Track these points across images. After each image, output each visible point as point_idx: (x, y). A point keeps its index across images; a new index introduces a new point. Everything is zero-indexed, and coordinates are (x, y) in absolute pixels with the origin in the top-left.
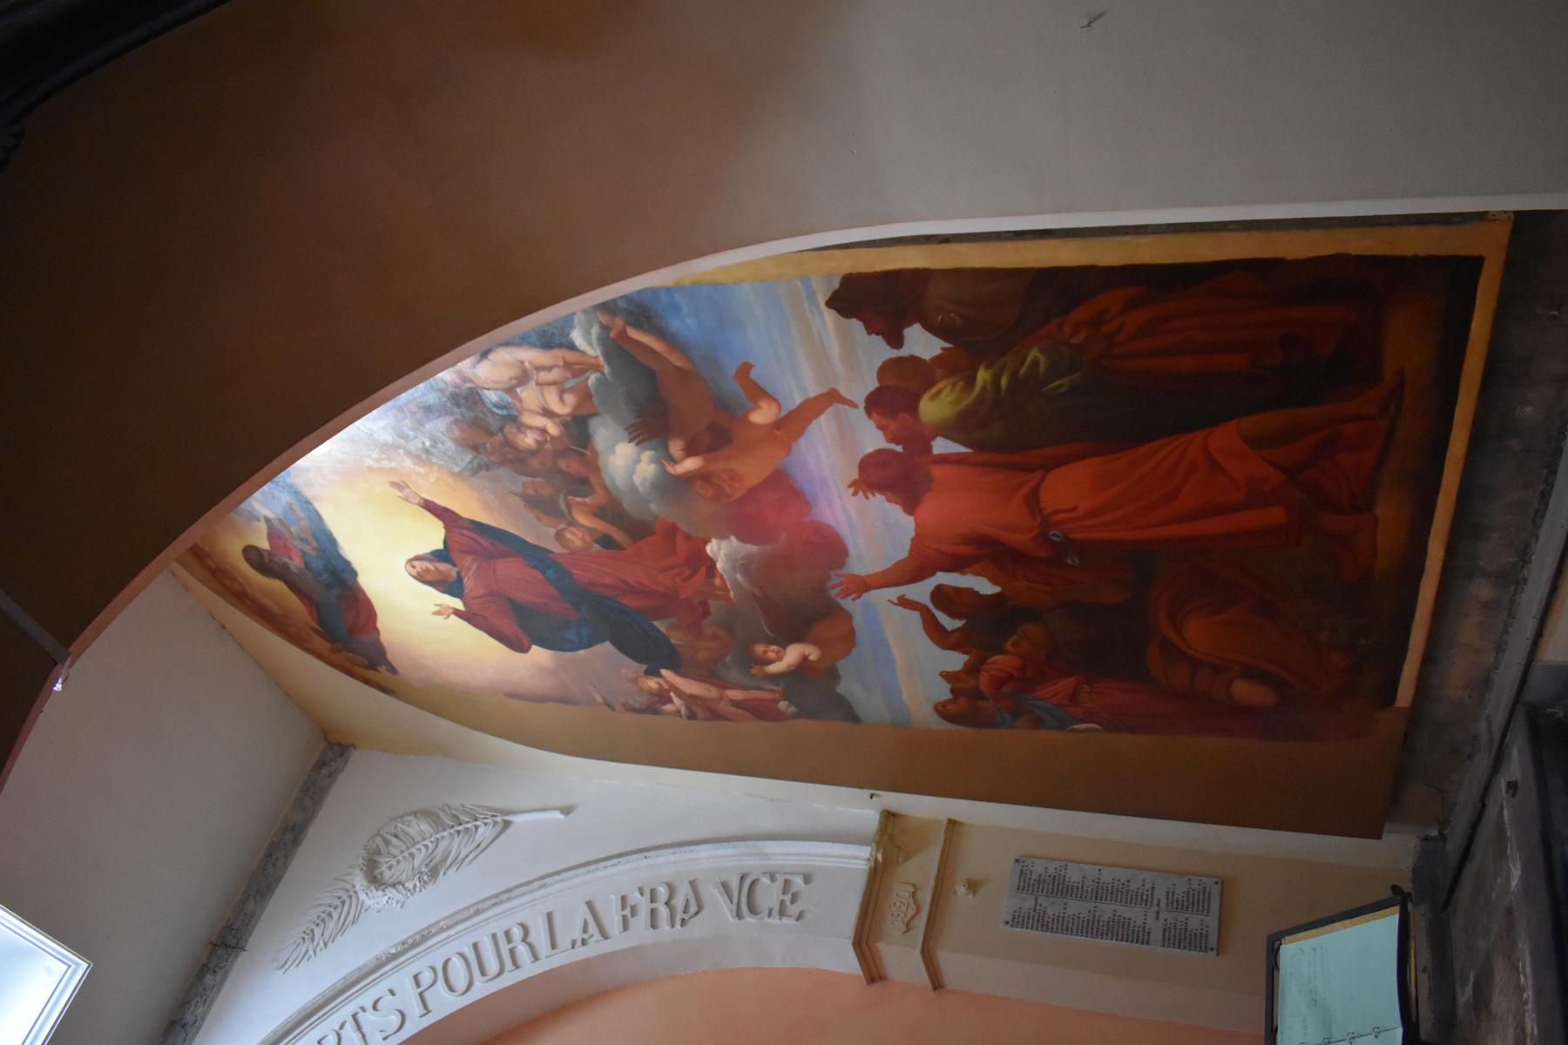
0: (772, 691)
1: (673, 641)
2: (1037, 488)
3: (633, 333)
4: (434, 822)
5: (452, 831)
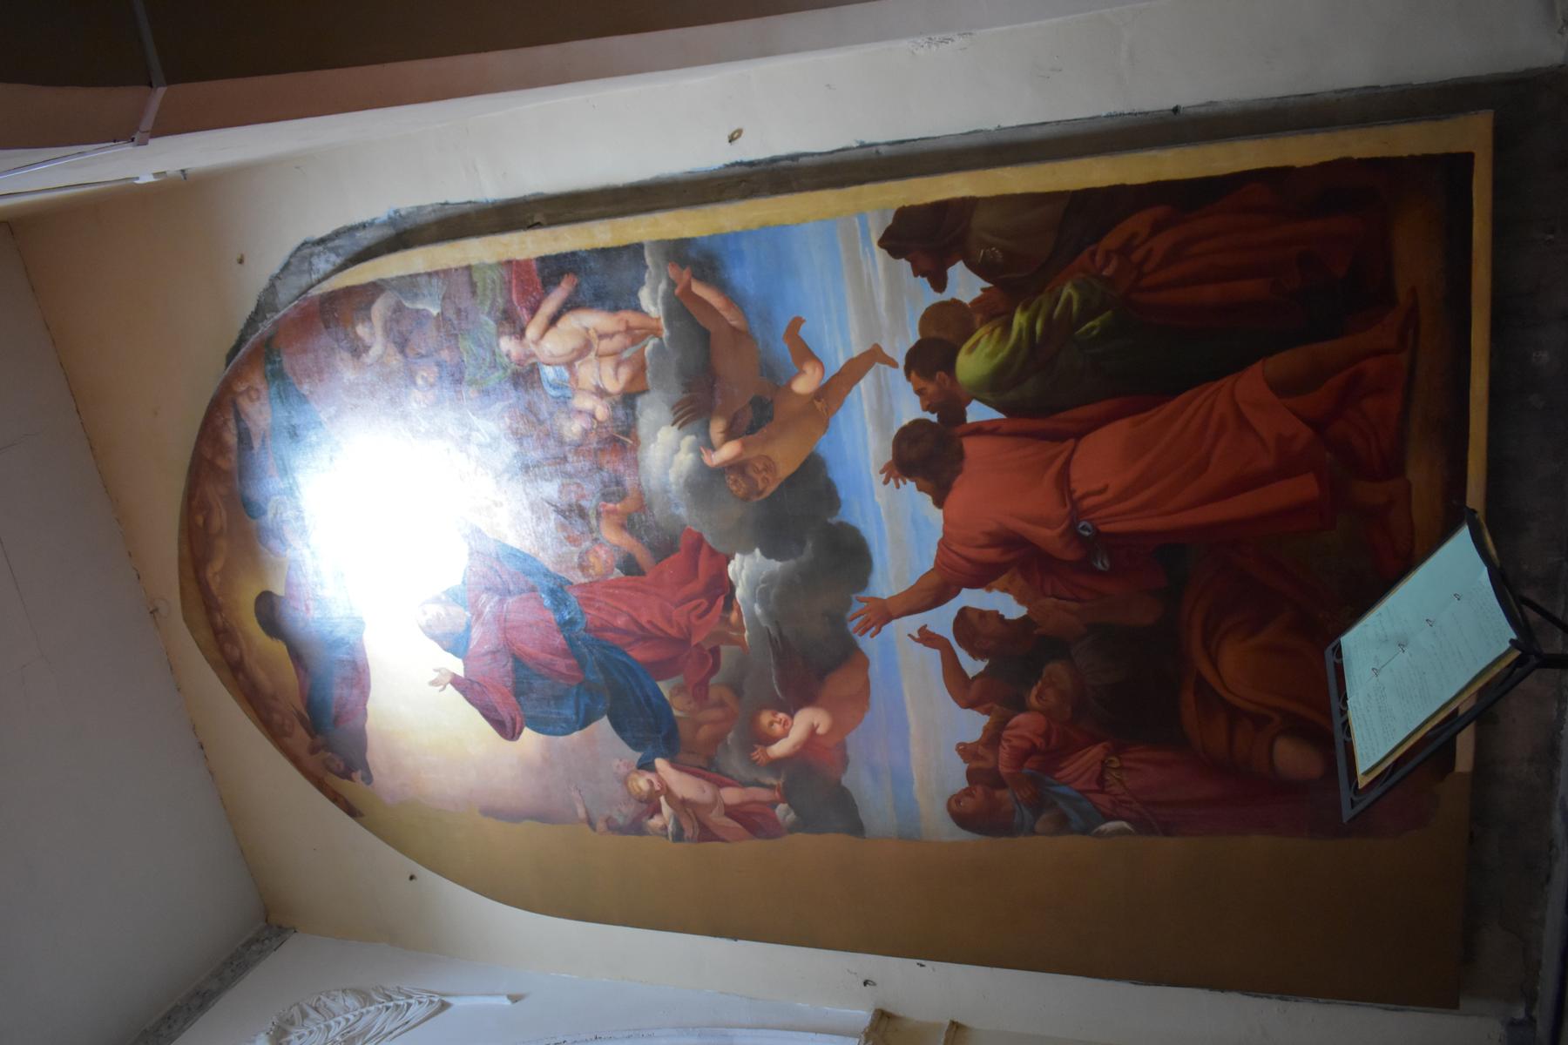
0: (771, 787)
1: (676, 713)
2: (1068, 463)
3: (699, 289)
4: (363, 998)
5: (380, 1006)
